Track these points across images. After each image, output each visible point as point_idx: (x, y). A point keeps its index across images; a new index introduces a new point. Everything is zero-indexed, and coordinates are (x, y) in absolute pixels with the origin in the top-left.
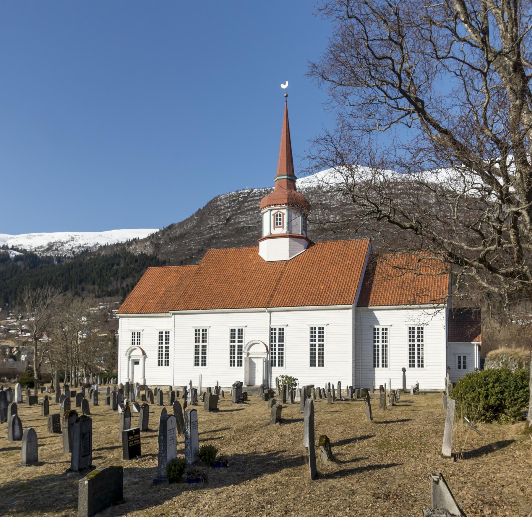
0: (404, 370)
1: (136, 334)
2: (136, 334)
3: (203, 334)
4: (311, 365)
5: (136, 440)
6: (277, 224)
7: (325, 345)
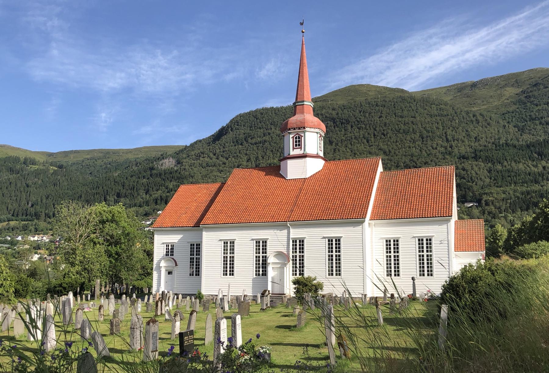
0: (413, 279)
1: (392, 241)
2: (392, 241)
3: (259, 249)
5: (190, 340)
6: (296, 145)
7: (385, 252)
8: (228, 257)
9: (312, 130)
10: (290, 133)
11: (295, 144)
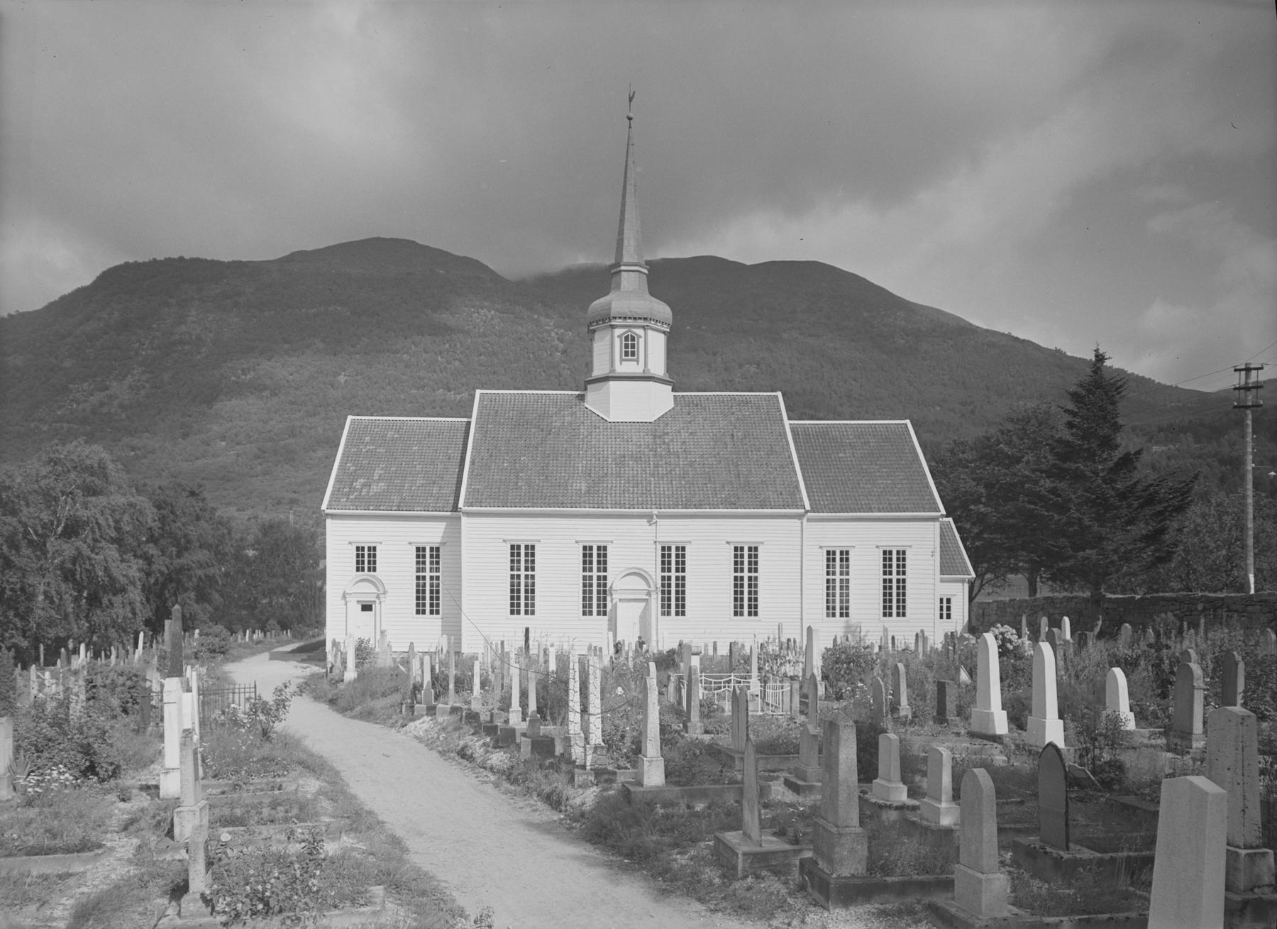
4: (512, 612)
6: (626, 354)
8: (523, 578)
9: (658, 326)
11: (624, 350)
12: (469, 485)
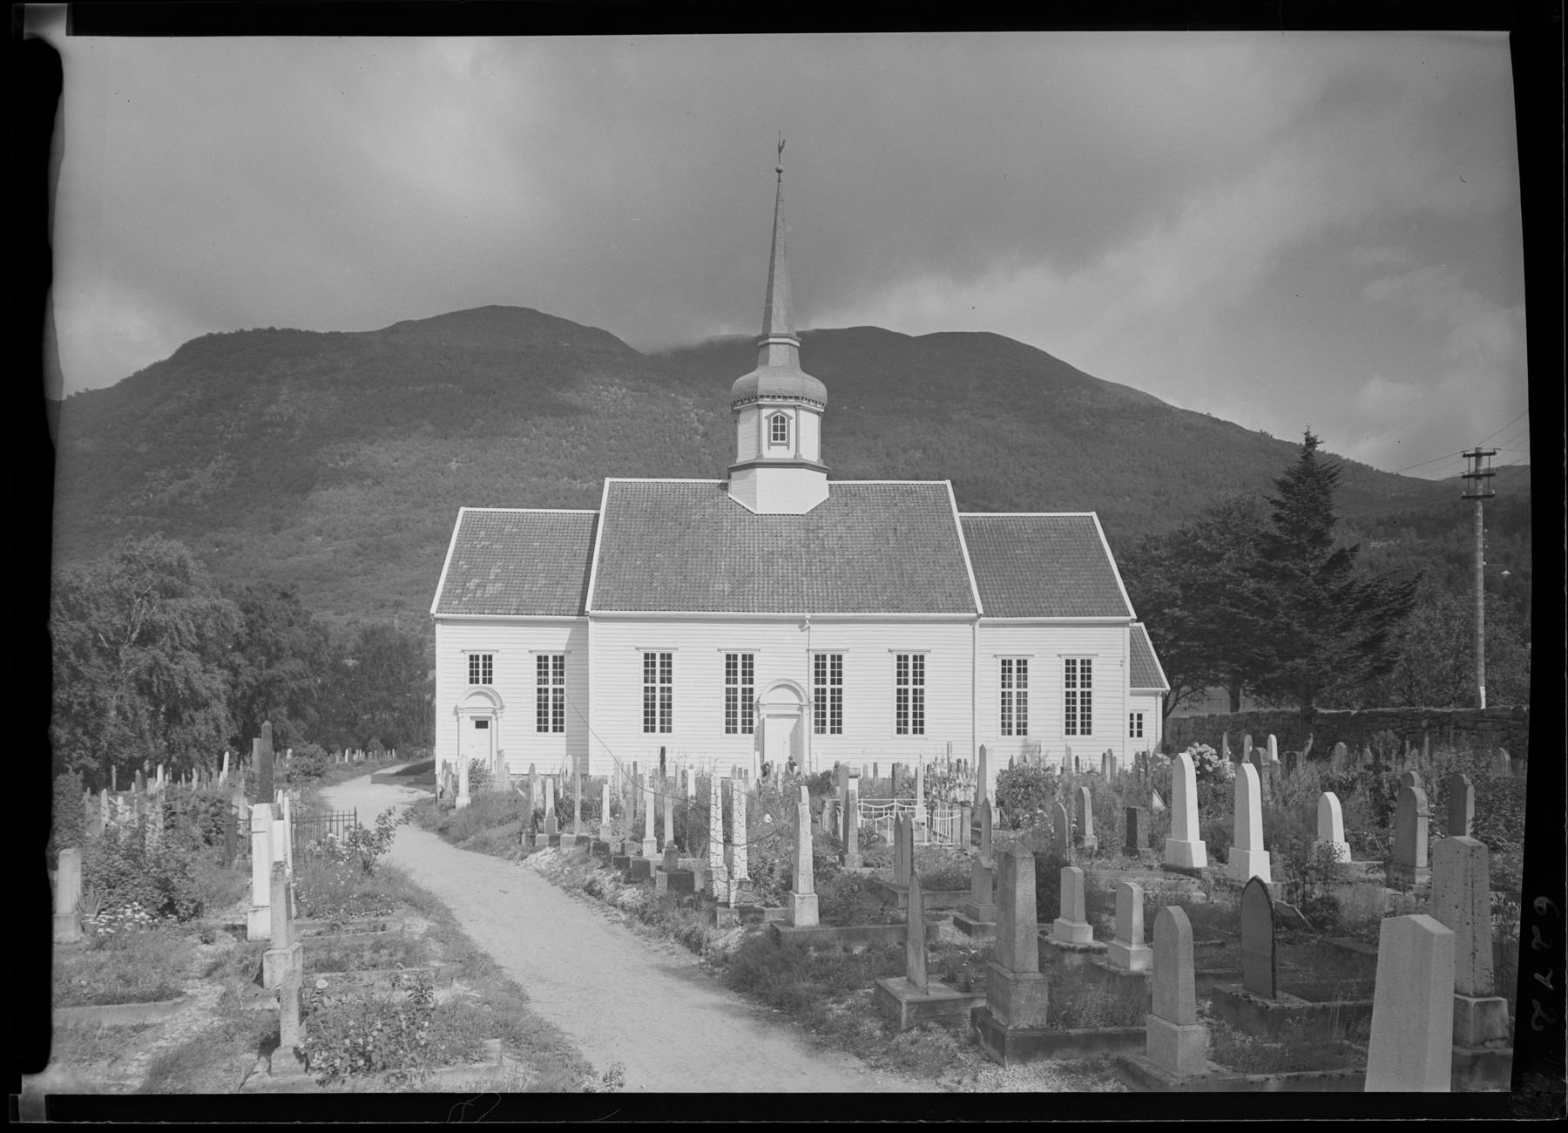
1: (551, 659)
2: (551, 659)
6: (775, 437)
8: (1078, 695)
10: (760, 407)
12: (597, 586)
